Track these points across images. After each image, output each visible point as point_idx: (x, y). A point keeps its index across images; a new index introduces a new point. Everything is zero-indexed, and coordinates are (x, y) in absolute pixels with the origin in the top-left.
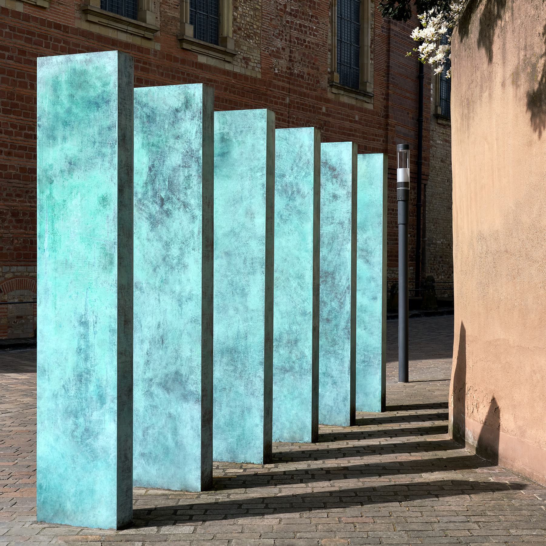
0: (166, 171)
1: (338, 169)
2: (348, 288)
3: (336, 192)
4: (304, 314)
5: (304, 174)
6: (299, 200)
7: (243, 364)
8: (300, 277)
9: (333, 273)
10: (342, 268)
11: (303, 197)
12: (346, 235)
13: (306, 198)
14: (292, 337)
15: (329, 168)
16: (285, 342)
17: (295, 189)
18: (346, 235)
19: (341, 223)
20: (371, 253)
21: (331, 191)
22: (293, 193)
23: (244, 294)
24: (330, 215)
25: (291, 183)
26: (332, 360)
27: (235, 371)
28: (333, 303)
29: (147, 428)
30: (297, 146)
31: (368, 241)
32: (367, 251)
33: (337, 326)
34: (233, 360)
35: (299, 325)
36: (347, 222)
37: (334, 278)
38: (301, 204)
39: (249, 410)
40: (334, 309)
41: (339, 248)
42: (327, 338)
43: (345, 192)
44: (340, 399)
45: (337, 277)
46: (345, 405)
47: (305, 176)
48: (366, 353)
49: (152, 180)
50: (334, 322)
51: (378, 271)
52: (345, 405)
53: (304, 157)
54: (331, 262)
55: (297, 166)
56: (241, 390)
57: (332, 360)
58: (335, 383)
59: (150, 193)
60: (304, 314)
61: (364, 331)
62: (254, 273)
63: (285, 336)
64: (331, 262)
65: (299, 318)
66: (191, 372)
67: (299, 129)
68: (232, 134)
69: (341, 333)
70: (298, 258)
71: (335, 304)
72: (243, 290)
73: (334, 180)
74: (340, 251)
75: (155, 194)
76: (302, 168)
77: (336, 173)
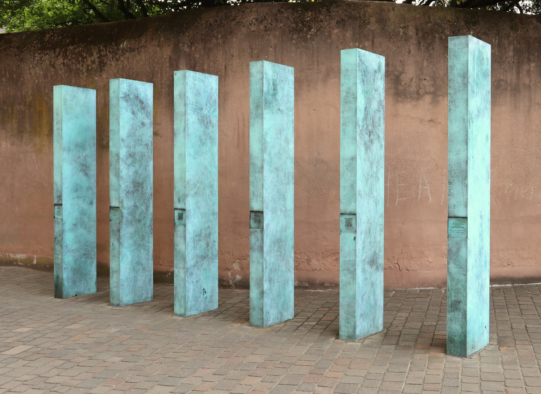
0: (372, 113)
1: (145, 103)
2: (151, 195)
3: (144, 121)
4: (213, 214)
5: (213, 109)
6: (211, 129)
7: (284, 249)
8: (212, 186)
9: (142, 184)
10: (148, 179)
11: (213, 127)
12: (150, 154)
13: (215, 128)
14: (207, 232)
15: (140, 101)
16: (203, 236)
17: (208, 120)
18: (150, 154)
19: (147, 145)
20: (89, 167)
21: (141, 120)
22: (207, 123)
23: (285, 199)
24: (140, 139)
25: (206, 115)
26: (142, 251)
27: (280, 255)
28: (142, 207)
29: (363, 295)
30: (209, 88)
31: (87, 158)
32: (86, 166)
33: (145, 224)
34: (280, 248)
35: (211, 222)
36: (150, 144)
37: (142, 188)
38: (212, 132)
39: (288, 281)
40: (143, 211)
41: (146, 164)
42: (139, 235)
43: (149, 121)
44: (147, 280)
45: (145, 187)
46: (150, 285)
47: (214, 112)
48: (86, 248)
49: (365, 118)
50: (143, 222)
51: (94, 182)
52: (150, 285)
53: (213, 97)
54: (141, 175)
55: (209, 103)
56: (284, 268)
57: (142, 251)
58: (144, 269)
59: (365, 127)
60: (213, 214)
61: (84, 230)
62: (288, 183)
63: (203, 231)
64: (141, 175)
65: (211, 217)
66: (380, 251)
67: (210, 75)
68: (278, 81)
69: (147, 230)
70: (210, 173)
71: (143, 208)
72: (284, 195)
73: (143, 111)
74: (146, 167)
75: (367, 128)
76: (212, 105)
77: (144, 106)
